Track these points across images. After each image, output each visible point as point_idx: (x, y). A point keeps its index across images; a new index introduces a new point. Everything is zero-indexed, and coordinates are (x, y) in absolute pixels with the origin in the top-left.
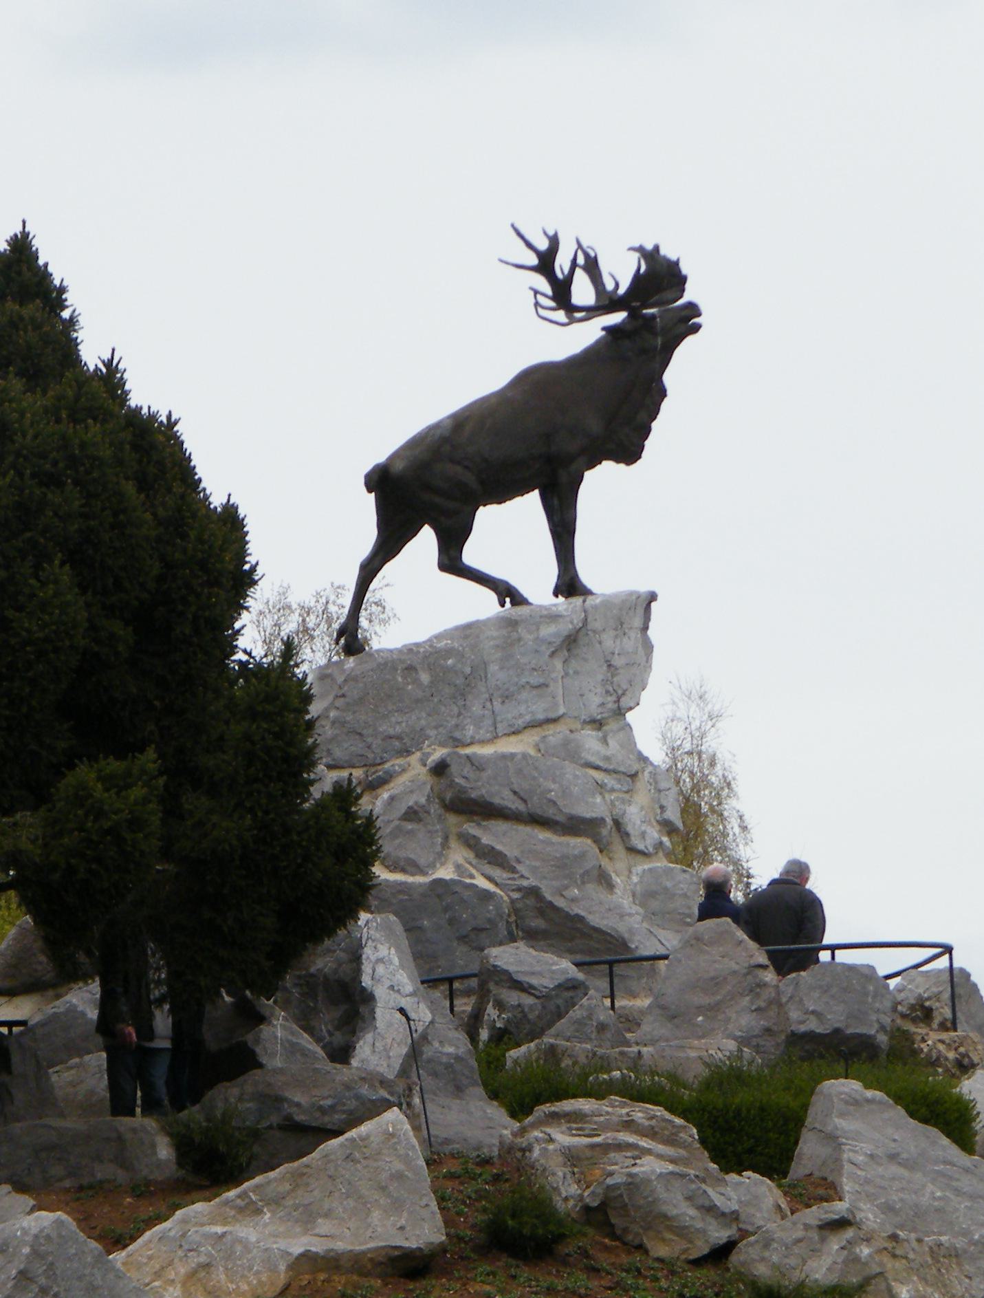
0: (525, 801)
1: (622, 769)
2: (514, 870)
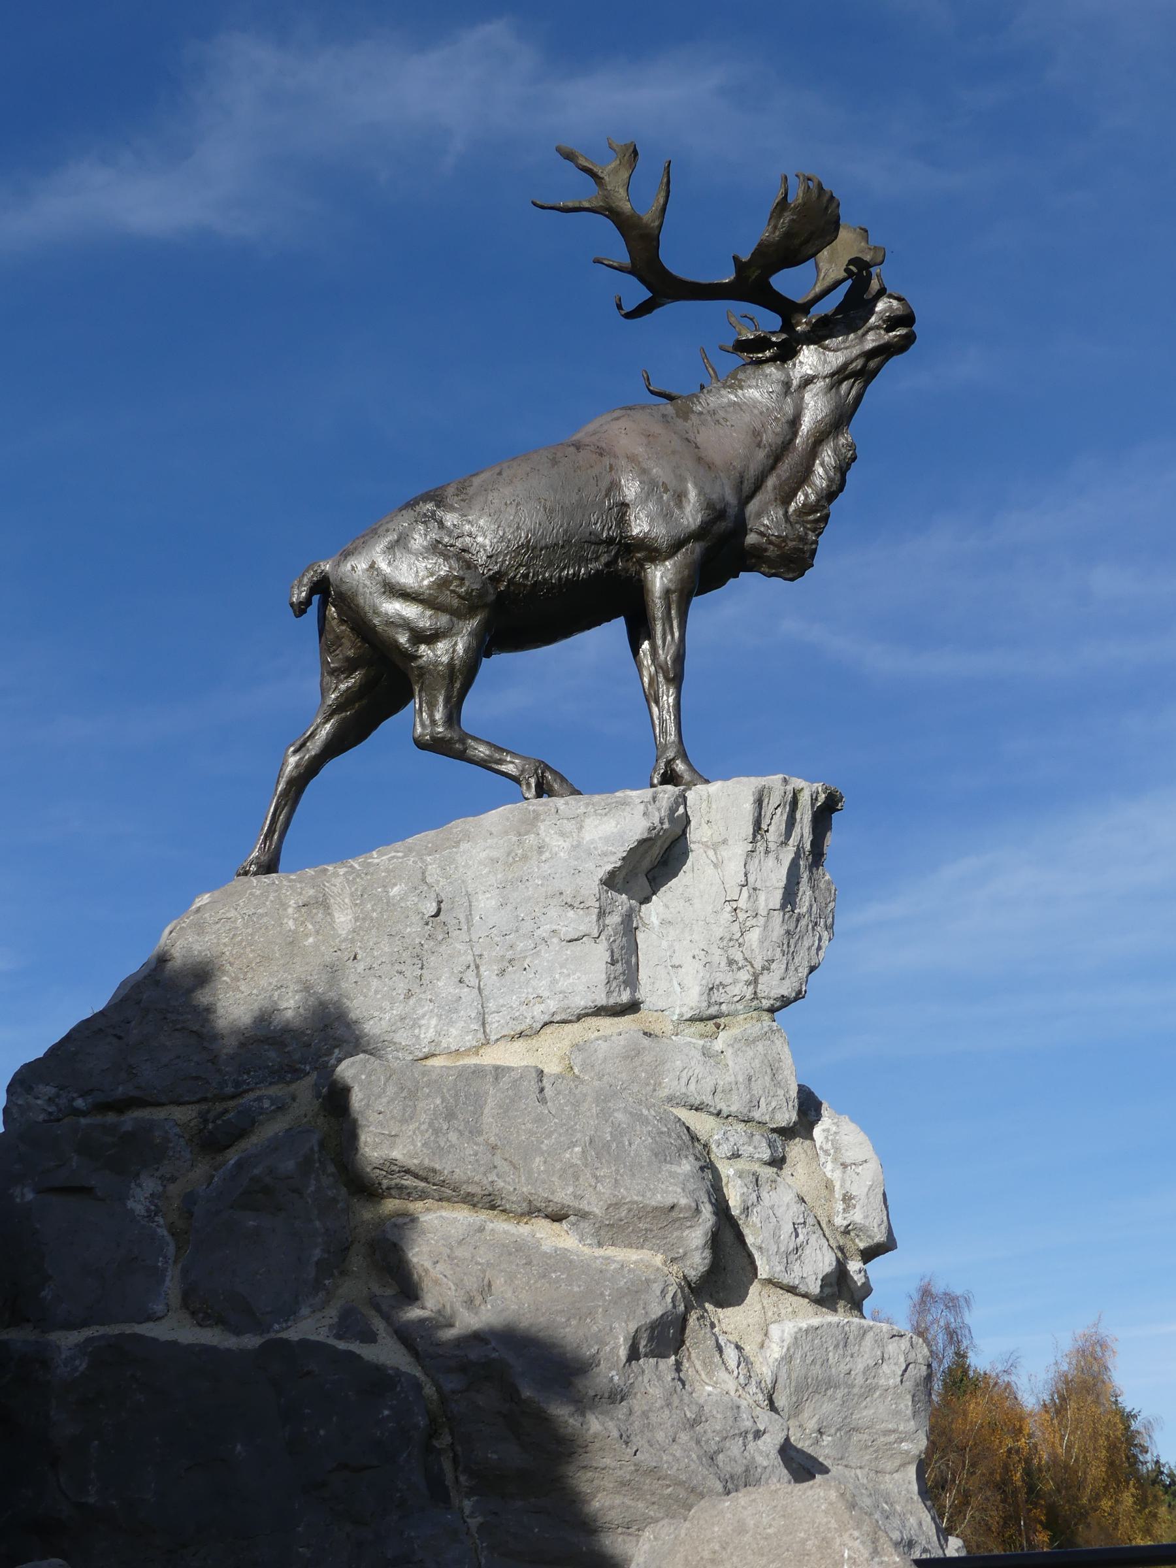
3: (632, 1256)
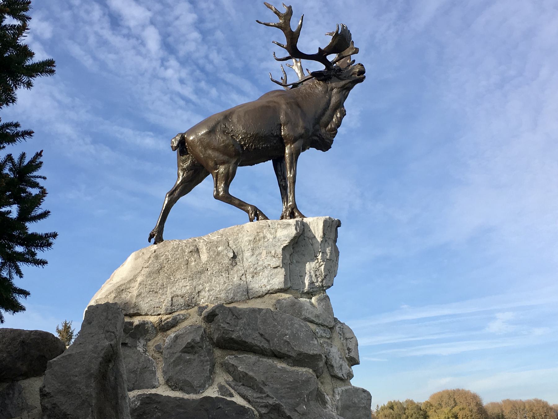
0: (268, 341)
1: (326, 324)
2: (262, 392)
3: (304, 370)
